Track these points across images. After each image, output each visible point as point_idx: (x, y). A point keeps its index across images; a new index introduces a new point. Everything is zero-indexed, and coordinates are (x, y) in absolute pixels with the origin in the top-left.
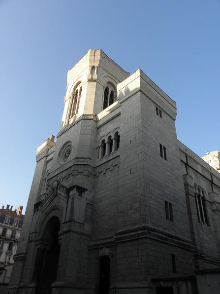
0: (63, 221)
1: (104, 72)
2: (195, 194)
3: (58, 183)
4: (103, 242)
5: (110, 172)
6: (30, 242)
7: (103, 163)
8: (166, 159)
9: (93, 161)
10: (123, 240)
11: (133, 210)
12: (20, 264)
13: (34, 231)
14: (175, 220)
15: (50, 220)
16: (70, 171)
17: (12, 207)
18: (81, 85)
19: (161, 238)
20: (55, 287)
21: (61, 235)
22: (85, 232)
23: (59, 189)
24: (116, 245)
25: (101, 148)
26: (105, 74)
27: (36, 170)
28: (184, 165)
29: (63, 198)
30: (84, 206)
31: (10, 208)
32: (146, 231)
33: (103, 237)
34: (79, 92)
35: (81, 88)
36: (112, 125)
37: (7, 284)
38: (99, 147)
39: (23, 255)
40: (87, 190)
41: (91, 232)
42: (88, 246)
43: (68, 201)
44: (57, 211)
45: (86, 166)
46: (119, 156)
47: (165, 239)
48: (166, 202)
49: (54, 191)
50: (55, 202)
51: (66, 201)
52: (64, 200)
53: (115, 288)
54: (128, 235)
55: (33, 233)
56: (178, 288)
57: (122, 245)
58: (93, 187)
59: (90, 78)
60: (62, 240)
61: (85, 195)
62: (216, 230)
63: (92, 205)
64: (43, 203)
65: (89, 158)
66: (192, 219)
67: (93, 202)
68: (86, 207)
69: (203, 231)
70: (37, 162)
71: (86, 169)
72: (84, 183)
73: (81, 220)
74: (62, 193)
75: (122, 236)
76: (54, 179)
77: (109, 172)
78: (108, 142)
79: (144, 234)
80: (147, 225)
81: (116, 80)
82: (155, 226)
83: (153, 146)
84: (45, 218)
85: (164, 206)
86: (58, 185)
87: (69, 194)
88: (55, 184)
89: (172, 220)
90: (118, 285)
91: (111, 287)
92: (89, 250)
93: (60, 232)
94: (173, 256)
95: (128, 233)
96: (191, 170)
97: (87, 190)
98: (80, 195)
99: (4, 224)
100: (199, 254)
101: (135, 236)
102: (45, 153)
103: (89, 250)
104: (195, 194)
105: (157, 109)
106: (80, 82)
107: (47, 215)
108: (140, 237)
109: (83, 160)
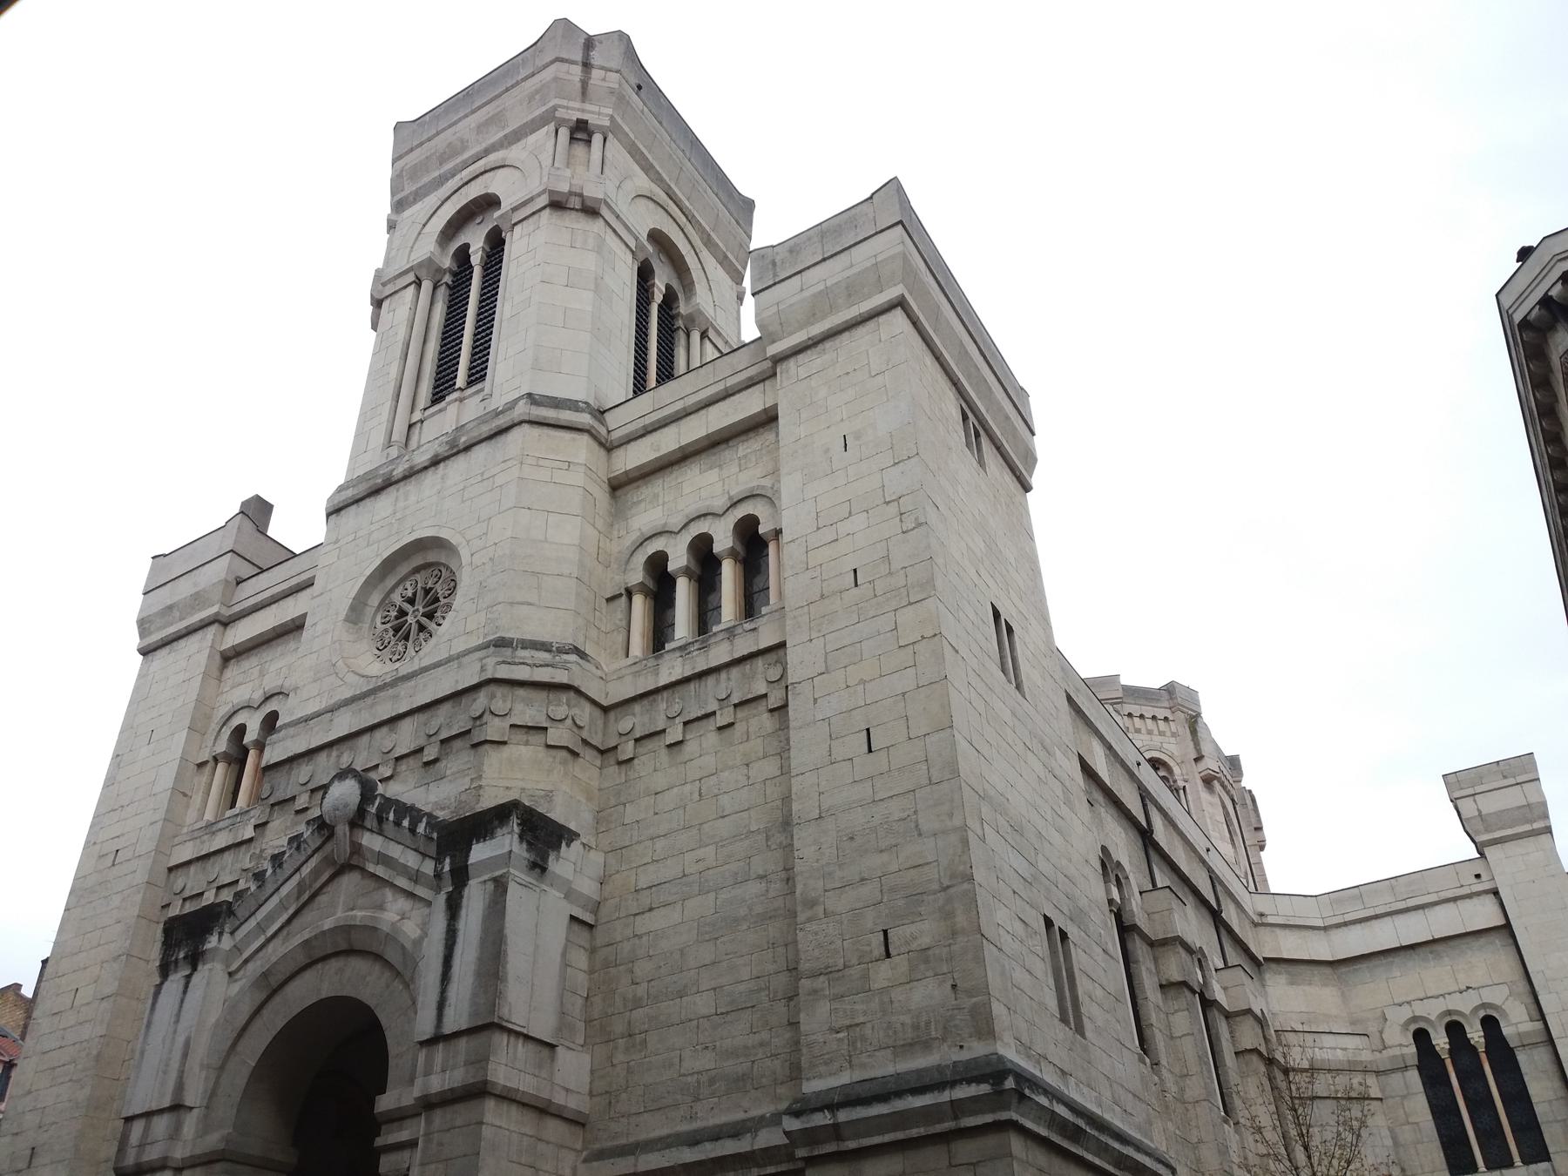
0: (425, 1025)
5: (712, 739)
7: (663, 681)
10: (852, 1145)
13: (166, 1103)
16: (450, 721)
22: (559, 1099)
23: (370, 822)
25: (638, 600)
26: (642, 182)
30: (556, 931)
33: (685, 1127)
36: (713, 475)
38: (629, 593)
40: (572, 836)
41: (591, 1094)
45: (564, 697)
55: (148, 1115)
61: (564, 863)
62: (1182, 1090)
64: (241, 912)
70: (145, 652)
71: (560, 711)
72: (549, 796)
75: (843, 1116)
76: (303, 772)
81: (689, 229)
88: (346, 793)
89: (1080, 1030)
95: (883, 1098)
97: (572, 836)
98: (539, 867)
101: (927, 1114)
107: (272, 987)
109: (544, 656)
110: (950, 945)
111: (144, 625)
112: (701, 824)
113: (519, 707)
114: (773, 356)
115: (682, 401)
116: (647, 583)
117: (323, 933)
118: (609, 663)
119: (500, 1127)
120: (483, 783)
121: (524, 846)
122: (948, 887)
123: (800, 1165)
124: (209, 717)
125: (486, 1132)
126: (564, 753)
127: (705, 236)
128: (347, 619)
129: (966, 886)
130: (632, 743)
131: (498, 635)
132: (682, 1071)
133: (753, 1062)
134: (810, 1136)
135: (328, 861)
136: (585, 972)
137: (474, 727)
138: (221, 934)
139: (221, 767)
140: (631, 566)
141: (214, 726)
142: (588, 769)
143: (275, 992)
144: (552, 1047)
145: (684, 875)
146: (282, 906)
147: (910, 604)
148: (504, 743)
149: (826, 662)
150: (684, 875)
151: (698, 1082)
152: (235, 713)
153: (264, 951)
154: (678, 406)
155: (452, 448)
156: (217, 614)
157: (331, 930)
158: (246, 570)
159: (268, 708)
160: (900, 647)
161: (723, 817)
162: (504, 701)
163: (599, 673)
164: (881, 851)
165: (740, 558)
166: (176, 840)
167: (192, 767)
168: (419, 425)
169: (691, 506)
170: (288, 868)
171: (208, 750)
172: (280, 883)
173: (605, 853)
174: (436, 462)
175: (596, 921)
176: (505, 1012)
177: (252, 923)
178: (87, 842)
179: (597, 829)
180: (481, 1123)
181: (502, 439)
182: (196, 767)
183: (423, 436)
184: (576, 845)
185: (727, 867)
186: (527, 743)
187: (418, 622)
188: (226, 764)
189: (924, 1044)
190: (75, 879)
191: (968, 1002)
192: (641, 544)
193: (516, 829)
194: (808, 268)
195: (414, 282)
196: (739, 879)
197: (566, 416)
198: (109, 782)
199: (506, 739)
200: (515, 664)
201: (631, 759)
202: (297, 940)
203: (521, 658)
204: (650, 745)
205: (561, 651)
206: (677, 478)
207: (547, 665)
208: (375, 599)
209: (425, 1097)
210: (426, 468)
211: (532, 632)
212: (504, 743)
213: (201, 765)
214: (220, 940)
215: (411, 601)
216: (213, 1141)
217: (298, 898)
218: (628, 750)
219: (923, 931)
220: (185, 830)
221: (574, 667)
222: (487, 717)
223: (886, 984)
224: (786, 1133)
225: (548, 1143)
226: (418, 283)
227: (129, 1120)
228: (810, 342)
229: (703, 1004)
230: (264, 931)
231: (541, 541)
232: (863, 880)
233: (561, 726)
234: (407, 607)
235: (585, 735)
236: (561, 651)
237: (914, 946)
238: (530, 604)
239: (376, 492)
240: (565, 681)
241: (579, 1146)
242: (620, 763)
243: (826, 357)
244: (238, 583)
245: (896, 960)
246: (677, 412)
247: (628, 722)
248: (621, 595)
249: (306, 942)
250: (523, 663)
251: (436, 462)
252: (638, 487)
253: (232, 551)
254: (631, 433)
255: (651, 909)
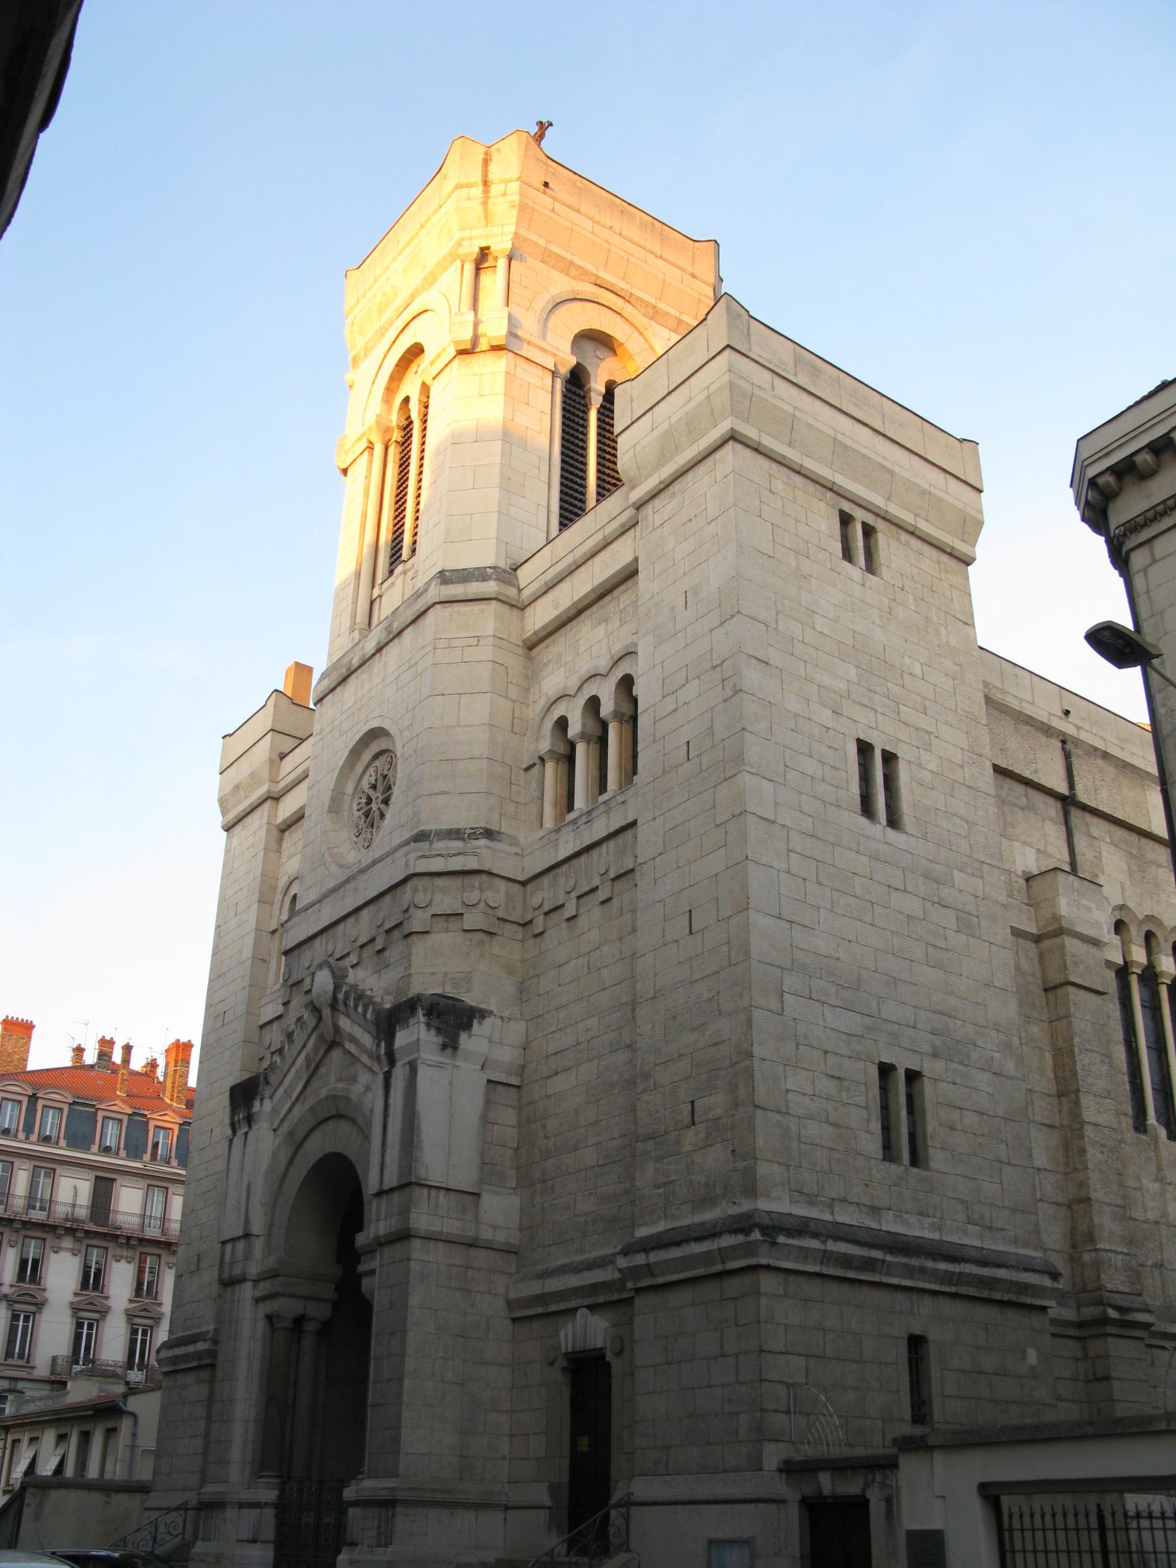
1: (555, 274)
2: (1123, 973)
3: (339, 979)
4: (574, 1281)
5: (597, 912)
6: (229, 1283)
7: (562, 855)
8: (894, 821)
9: (514, 842)
11: (700, 1127)
12: (194, 1388)
13: (241, 1234)
14: (937, 1158)
15: (312, 1169)
16: (388, 912)
17: (128, 1049)
18: (423, 369)
19: (845, 1261)
20: (356, 1504)
21: (371, 1251)
22: (486, 1234)
23: (341, 1007)
24: (630, 1301)
27: (217, 976)
28: (1053, 809)
29: (365, 1059)
30: (471, 1100)
31: (117, 1057)
32: (756, 1235)
33: (578, 1258)
34: (415, 416)
35: (425, 389)
36: (600, 632)
37: (143, 1489)
38: (542, 760)
39: (201, 1346)
40: (482, 1014)
41: (520, 1229)
42: (511, 1304)
43: (387, 1077)
44: (344, 1126)
45: (476, 880)
46: (634, 824)
47: (869, 1264)
48: (885, 1070)
49: (320, 1019)
50: (329, 1083)
51: (381, 1077)
52: (371, 1070)
53: (629, 1503)
54: (675, 1253)
55: (233, 1240)
56: (888, 1501)
57: (652, 1299)
58: (523, 993)
59: (467, 335)
60: (376, 1280)
61: (474, 1041)
63: (518, 1087)
65: (489, 834)
66: (1082, 1123)
67: (521, 1070)
68: (487, 1102)
69: (1160, 1179)
70: (228, 828)
71: (474, 897)
72: (468, 978)
73: (464, 1178)
74: (358, 1032)
75: (655, 1257)
76: (319, 949)
77: (592, 914)
78: (583, 736)
79: (749, 1249)
80: (763, 1205)
82: (812, 1204)
83: (810, 767)
84: (291, 1161)
85: (875, 1091)
86: (337, 988)
87: (390, 1038)
88: (323, 981)
90: (641, 1488)
91: (615, 1498)
92: (514, 1320)
93: (361, 1239)
94: (916, 1342)
96: (1098, 827)
97: (482, 1014)
98: (450, 1045)
99: (92, 1156)
100: (1113, 1314)
101: (706, 1258)
102: (265, 775)
103: (514, 1320)
104: (1123, 973)
105: (845, 520)
106: (416, 351)
108: (733, 1265)
109: (458, 845)
110: (733, 1115)
111: (223, 803)
112: (589, 996)
113: (438, 897)
114: (634, 503)
115: (572, 554)
116: (556, 749)
117: (321, 1101)
118: (528, 837)
119: (428, 1262)
120: (412, 971)
121: (433, 1032)
122: (736, 1063)
123: (632, 1294)
124: (274, 888)
125: (413, 1265)
126: (479, 936)
127: (651, 311)
128: (330, 811)
129: (747, 1063)
130: (542, 917)
131: (420, 829)
132: (576, 1212)
133: (620, 1206)
134: (634, 1272)
135: (321, 1038)
136: (514, 1127)
137: (405, 919)
138: (262, 1100)
139: (550, 766)
140: (542, 734)
141: (279, 897)
142: (508, 947)
143: (299, 1146)
144: (478, 1195)
145: (578, 1044)
146: (298, 1076)
147: (726, 779)
148: (427, 932)
149: (664, 842)
150: (578, 1044)
151: (586, 1221)
152: (291, 883)
153: (292, 1113)
154: (569, 560)
155: (389, 633)
156: (269, 791)
157: (326, 1098)
158: (287, 744)
159: (619, 673)
160: (717, 825)
161: (604, 990)
162: (425, 894)
163: (514, 850)
164: (694, 1030)
165: (625, 718)
166: (263, 1001)
167: (266, 936)
168: (378, 599)
169: (584, 667)
170: (298, 1043)
171: (275, 919)
172: (294, 1056)
173: (527, 1021)
174: (379, 650)
175: (522, 1082)
176: (422, 1173)
177: (281, 1090)
178: (207, 1005)
179: (521, 998)
180: (409, 1260)
181: (421, 622)
182: (270, 935)
183: (382, 611)
184: (488, 1021)
185: (605, 1036)
186: (447, 930)
187: (379, 808)
188: (586, 744)
189: (709, 1201)
190: (203, 1036)
191: (741, 1164)
192: (549, 708)
193: (422, 1019)
194: (658, 403)
195: (368, 447)
196: (614, 1048)
197: (475, 588)
198: (215, 953)
199: (428, 929)
200: (432, 856)
201: (542, 933)
202: (307, 1105)
203: (438, 850)
204: (555, 918)
205: (474, 835)
206: (575, 636)
207: (459, 854)
208: (350, 788)
209: (377, 1237)
210: (374, 655)
211: (449, 821)
212: (427, 932)
213: (274, 932)
214: (262, 1105)
215: (374, 787)
216: (271, 1261)
217: (307, 1069)
218: (540, 921)
219: (715, 1103)
220: (268, 992)
221: (483, 851)
222: (412, 910)
223: (691, 1148)
224: (620, 1270)
225: (479, 1269)
226: (370, 447)
227: (224, 1243)
228: (662, 486)
229: (589, 1157)
230: (290, 1097)
231: (453, 727)
232: (680, 1055)
233: (474, 911)
234: (372, 793)
235: (501, 913)
236: (474, 835)
237: (710, 1116)
238: (446, 793)
239: (344, 680)
240: (475, 866)
241: (513, 1270)
242: (536, 936)
243: (675, 502)
244: (282, 759)
245: (698, 1127)
246: (569, 566)
247: (543, 895)
248: (534, 765)
249: (312, 1108)
250: (439, 855)
251: (379, 650)
252: (547, 646)
253: (272, 730)
254: (536, 591)
255: (557, 1073)
